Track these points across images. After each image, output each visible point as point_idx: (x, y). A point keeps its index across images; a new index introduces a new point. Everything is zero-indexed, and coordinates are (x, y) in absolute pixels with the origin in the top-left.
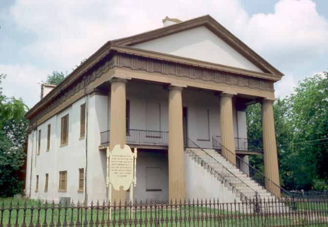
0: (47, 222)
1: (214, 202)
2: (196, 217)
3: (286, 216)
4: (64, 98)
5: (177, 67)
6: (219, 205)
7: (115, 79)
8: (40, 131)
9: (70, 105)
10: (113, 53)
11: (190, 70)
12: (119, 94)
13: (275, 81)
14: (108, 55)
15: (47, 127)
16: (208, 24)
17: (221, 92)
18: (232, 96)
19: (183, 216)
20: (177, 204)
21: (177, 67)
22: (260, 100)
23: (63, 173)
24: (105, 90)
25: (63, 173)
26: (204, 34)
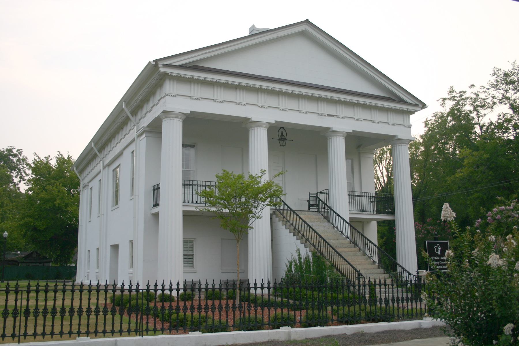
0: (111, 316)
1: (178, 287)
2: (11, 310)
3: (403, 303)
4: (112, 144)
5: (389, 114)
6: (387, 287)
7: (166, 113)
8: (91, 189)
9: (121, 154)
10: (165, 76)
11: (238, 94)
12: (173, 132)
13: (412, 113)
14: (154, 78)
15: (98, 183)
16: (307, 32)
17: (247, 120)
18: (345, 135)
19: (76, 304)
20: (202, 287)
21: (389, 114)
22: (391, 140)
23: (115, 247)
24: (155, 129)
25: (115, 247)
26: (302, 49)
